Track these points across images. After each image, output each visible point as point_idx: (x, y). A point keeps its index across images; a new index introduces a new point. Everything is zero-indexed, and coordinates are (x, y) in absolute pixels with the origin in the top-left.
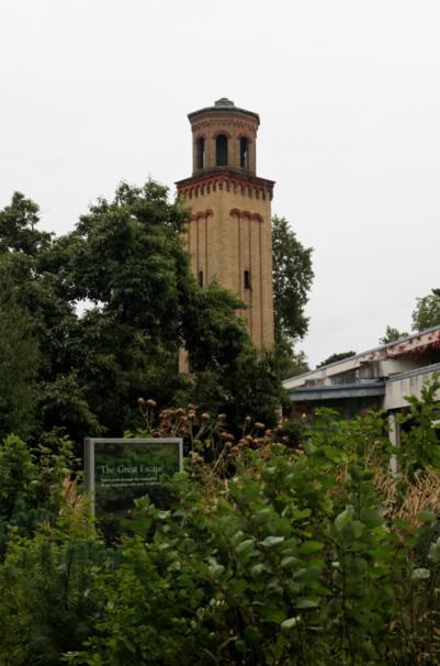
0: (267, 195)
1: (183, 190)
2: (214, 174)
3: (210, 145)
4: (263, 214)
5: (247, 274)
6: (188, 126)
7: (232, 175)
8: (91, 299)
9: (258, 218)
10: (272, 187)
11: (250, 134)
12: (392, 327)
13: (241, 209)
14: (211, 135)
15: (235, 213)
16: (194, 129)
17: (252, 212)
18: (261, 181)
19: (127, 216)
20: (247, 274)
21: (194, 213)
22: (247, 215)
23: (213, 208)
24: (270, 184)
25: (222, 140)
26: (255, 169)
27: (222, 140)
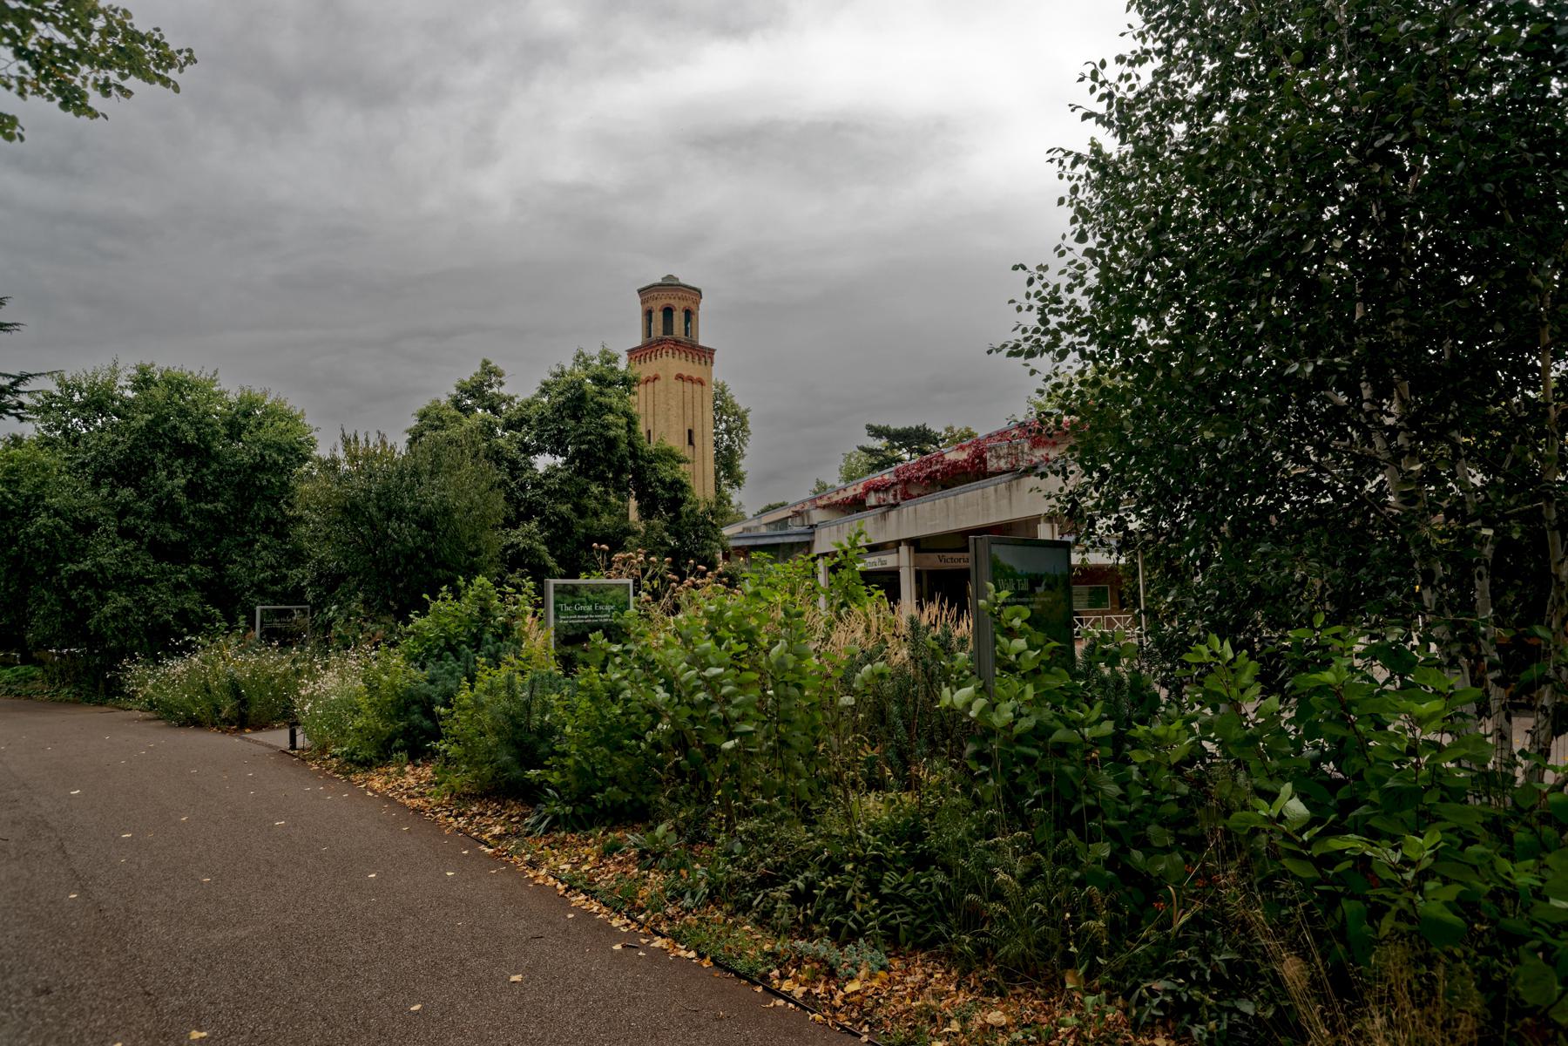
2: (661, 342)
3: (658, 317)
4: (705, 378)
5: (690, 432)
6: (638, 299)
7: (677, 343)
11: (693, 307)
15: (679, 377)
22: (691, 379)
24: (711, 352)
25: (668, 312)
27: (668, 312)
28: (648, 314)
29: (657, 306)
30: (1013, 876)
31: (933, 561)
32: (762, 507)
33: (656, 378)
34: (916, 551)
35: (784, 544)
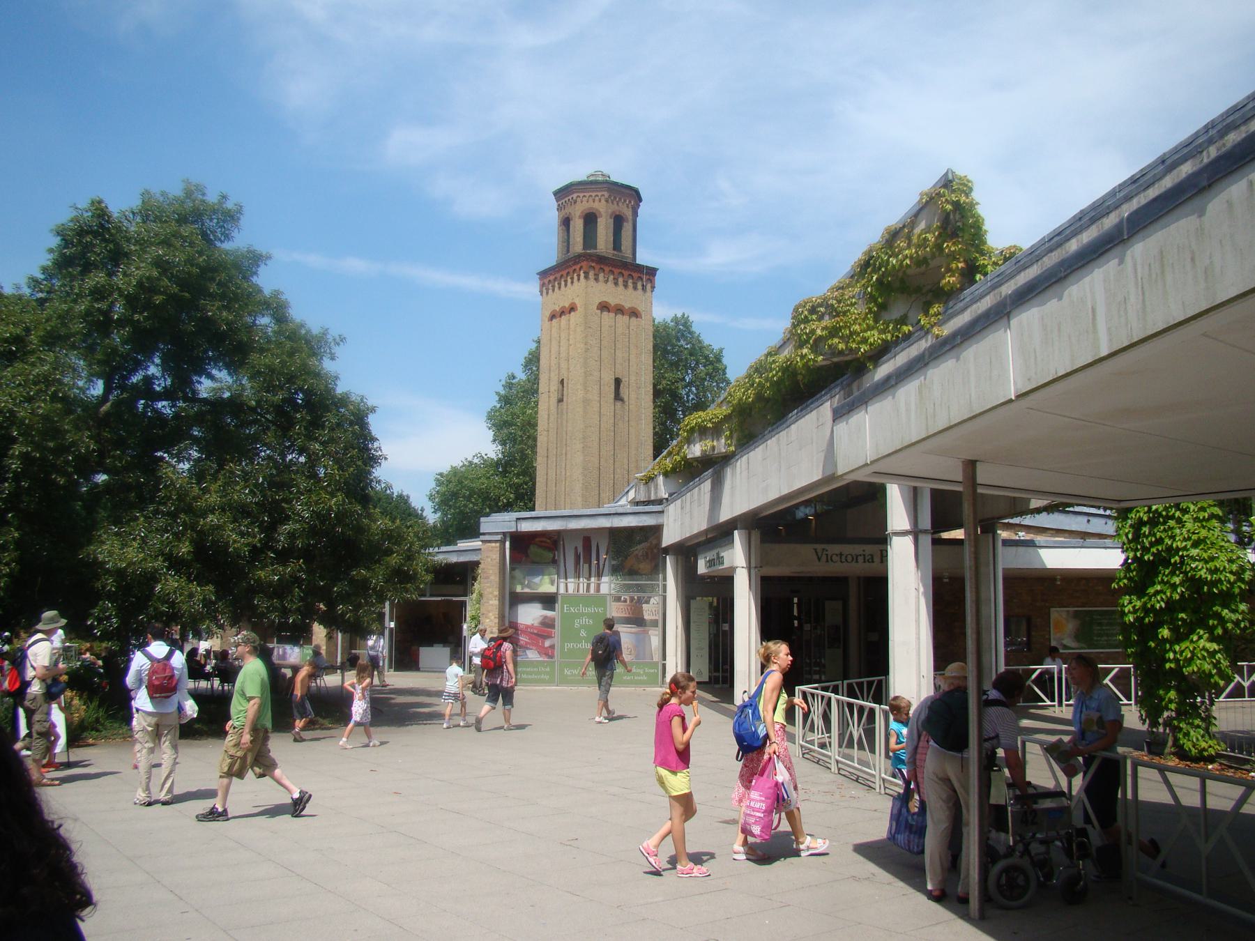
0: (649, 286)
1: (546, 281)
2: (578, 259)
3: (578, 226)
4: (641, 308)
5: (618, 382)
6: (554, 203)
7: (601, 260)
8: (131, 699)
9: (634, 313)
10: (654, 275)
11: (628, 213)
12: (724, 353)
13: (613, 301)
14: (578, 214)
15: (604, 307)
16: (559, 209)
17: (627, 305)
18: (640, 269)
19: (151, 578)
20: (618, 397)
21: (521, 376)
22: (619, 310)
23: (577, 301)
24: (652, 272)
25: (590, 219)
26: (944, 906)
27: (590, 219)
28: (566, 222)
29: (577, 211)
30: (313, 676)
31: (801, 560)
32: (1021, 550)
33: (572, 309)
34: (764, 540)
35: (1005, 610)
